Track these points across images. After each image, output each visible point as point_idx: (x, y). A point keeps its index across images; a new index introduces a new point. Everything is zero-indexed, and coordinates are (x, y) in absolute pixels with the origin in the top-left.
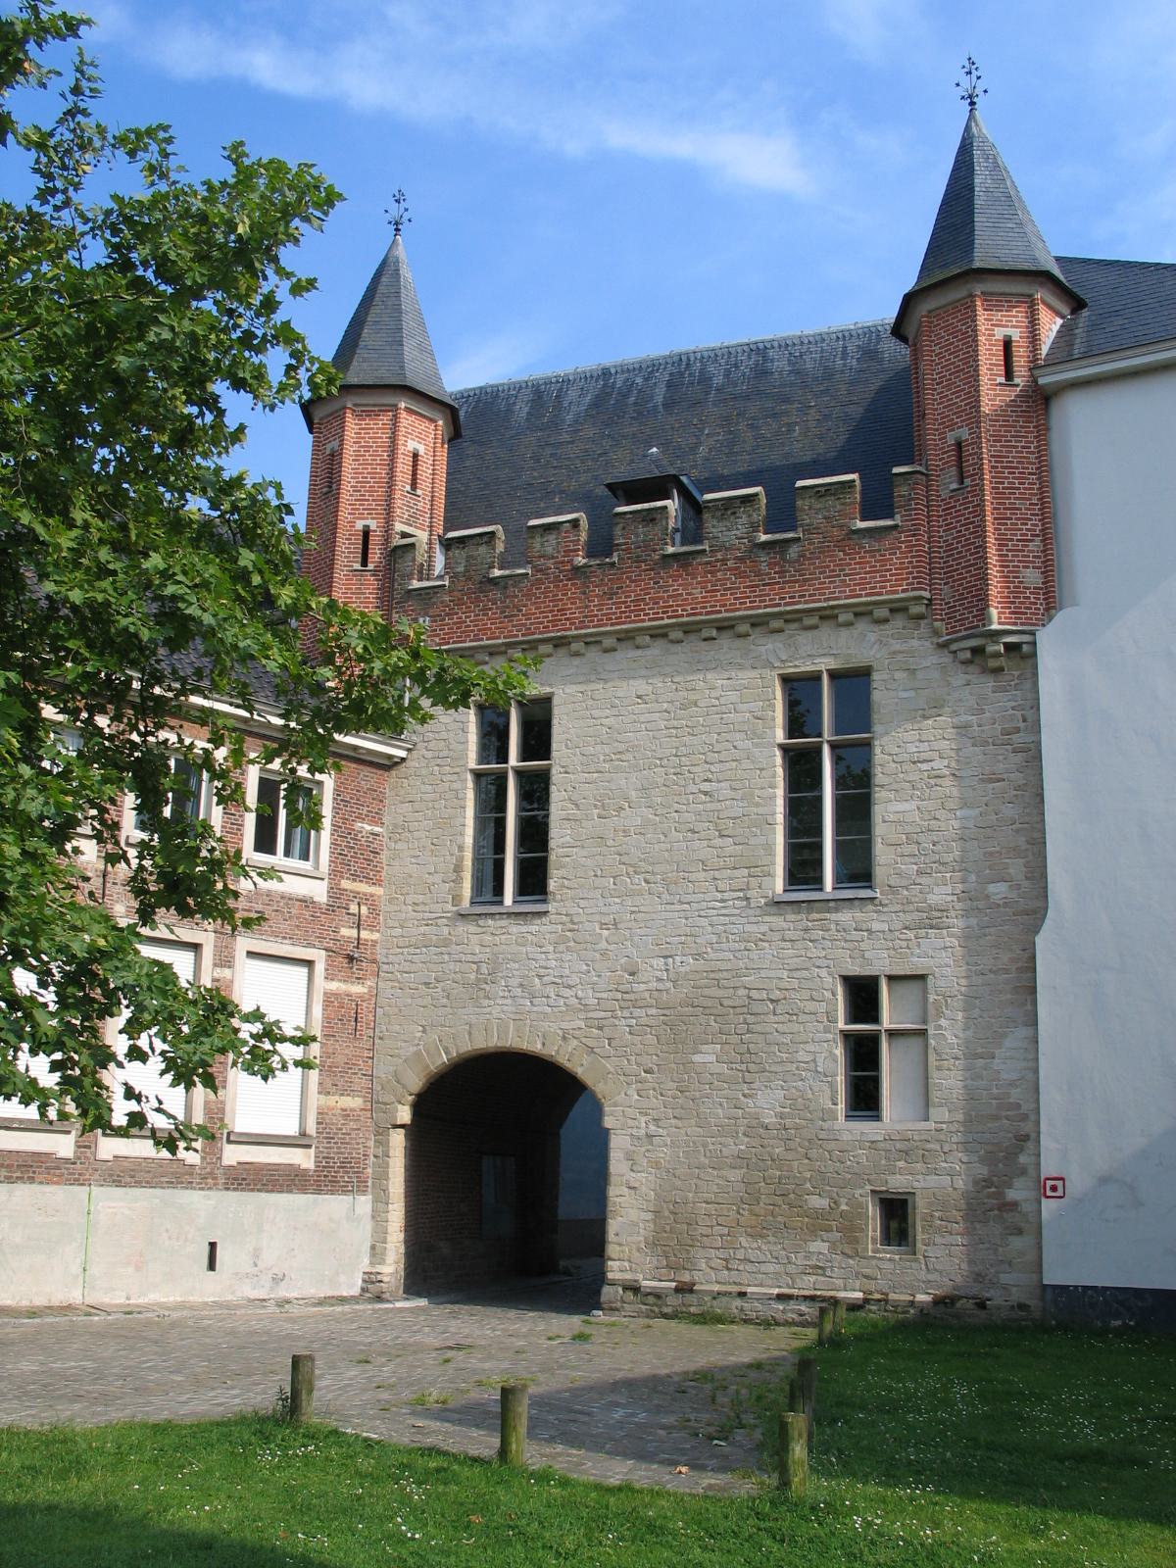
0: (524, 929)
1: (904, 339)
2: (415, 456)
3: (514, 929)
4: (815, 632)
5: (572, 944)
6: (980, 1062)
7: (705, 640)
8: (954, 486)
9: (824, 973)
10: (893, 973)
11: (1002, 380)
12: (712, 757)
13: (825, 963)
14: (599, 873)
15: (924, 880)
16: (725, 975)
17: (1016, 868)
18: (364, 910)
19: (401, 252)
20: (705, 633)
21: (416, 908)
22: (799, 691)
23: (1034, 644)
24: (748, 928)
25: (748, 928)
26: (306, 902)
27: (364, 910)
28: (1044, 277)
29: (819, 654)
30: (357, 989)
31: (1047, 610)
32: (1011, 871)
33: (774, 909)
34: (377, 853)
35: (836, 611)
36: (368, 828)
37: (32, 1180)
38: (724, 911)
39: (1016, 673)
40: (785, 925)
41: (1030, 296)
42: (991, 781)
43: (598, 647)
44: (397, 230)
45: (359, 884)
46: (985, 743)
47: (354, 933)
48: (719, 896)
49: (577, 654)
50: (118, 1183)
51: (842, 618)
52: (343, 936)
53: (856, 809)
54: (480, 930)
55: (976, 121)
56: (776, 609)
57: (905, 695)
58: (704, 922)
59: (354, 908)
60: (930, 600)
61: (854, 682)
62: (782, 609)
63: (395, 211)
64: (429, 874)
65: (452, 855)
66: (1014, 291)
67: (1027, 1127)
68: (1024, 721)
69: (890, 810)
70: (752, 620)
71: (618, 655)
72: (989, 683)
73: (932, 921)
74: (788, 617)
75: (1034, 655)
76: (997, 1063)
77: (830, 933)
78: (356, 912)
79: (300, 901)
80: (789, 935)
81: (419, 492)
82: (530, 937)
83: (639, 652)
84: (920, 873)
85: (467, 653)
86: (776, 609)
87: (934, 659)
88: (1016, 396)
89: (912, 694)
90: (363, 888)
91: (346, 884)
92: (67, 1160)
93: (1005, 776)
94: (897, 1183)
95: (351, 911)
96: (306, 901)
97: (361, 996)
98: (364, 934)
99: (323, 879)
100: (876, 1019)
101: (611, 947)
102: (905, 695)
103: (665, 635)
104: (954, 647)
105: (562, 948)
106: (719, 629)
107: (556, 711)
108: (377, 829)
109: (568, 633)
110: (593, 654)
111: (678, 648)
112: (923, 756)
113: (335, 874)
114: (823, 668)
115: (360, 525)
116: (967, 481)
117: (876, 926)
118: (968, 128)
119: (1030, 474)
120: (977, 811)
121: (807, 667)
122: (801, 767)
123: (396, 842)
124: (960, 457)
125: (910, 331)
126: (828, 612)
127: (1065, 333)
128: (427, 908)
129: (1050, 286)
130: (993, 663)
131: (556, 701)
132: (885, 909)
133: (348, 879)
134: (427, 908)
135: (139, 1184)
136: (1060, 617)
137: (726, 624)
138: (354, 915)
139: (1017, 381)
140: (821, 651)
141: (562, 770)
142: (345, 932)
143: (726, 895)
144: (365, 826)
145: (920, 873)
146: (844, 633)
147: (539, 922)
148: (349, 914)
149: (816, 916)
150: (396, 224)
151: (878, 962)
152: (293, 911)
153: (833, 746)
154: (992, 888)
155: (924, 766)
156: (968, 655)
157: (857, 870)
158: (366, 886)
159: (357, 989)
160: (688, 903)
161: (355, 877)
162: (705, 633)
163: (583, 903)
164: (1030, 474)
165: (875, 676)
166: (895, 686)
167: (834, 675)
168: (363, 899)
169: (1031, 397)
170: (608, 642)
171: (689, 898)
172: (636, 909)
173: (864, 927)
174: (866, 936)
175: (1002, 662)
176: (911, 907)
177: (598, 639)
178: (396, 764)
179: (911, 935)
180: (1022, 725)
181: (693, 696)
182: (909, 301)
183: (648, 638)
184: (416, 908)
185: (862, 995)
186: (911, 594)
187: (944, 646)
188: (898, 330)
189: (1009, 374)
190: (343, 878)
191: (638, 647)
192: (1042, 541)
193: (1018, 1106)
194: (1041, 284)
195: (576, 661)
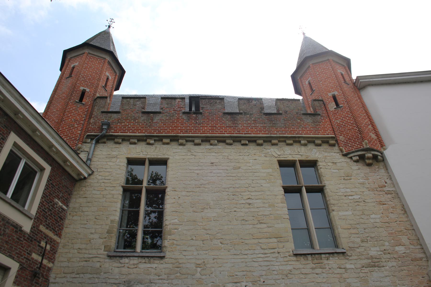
0: (149, 265)
2: (108, 79)
3: (142, 266)
4: (291, 147)
5: (178, 274)
12: (250, 189)
14: (194, 238)
18: (48, 247)
20: (243, 142)
21: (80, 251)
24: (281, 267)
25: (281, 267)
26: (17, 228)
27: (48, 247)
33: (294, 258)
34: (62, 219)
35: (300, 139)
36: (60, 204)
38: (266, 259)
40: (301, 266)
45: (49, 231)
46: (373, 190)
47: (39, 259)
48: (263, 251)
49: (181, 144)
52: (33, 259)
54: (120, 265)
58: (256, 264)
59: (43, 244)
64: (92, 233)
65: (107, 225)
71: (201, 147)
72: (367, 170)
77: (326, 269)
78: (44, 246)
79: (14, 226)
80: (304, 271)
82: (153, 270)
83: (212, 147)
85: (126, 138)
90: (51, 234)
91: (42, 228)
93: (386, 203)
95: (41, 245)
96: (17, 228)
98: (45, 262)
99: (31, 219)
101: (203, 277)
105: (172, 277)
106: (249, 141)
108: (64, 207)
109: (179, 135)
110: (190, 146)
112: (349, 194)
113: (38, 220)
114: (297, 159)
115: (82, 88)
117: (348, 266)
123: (73, 216)
126: (297, 139)
128: (87, 252)
130: (367, 161)
132: (350, 258)
133: (44, 225)
134: (87, 252)
138: (42, 247)
140: (295, 153)
141: (173, 190)
142: (34, 256)
143: (266, 251)
144: (59, 202)
145: (362, 241)
146: (303, 148)
147: (158, 262)
148: (39, 246)
149: (316, 261)
152: (7, 231)
154: (397, 248)
155: (350, 197)
156: (358, 158)
158: (53, 234)
160: (246, 255)
161: (48, 227)
163: (185, 253)
168: (50, 241)
170: (197, 141)
171: (246, 252)
172: (217, 257)
173: (342, 267)
175: (370, 161)
176: (363, 257)
177: (193, 139)
178: (81, 179)
179: (366, 270)
181: (238, 165)
183: (216, 141)
184: (80, 251)
190: (42, 224)
191: (211, 145)
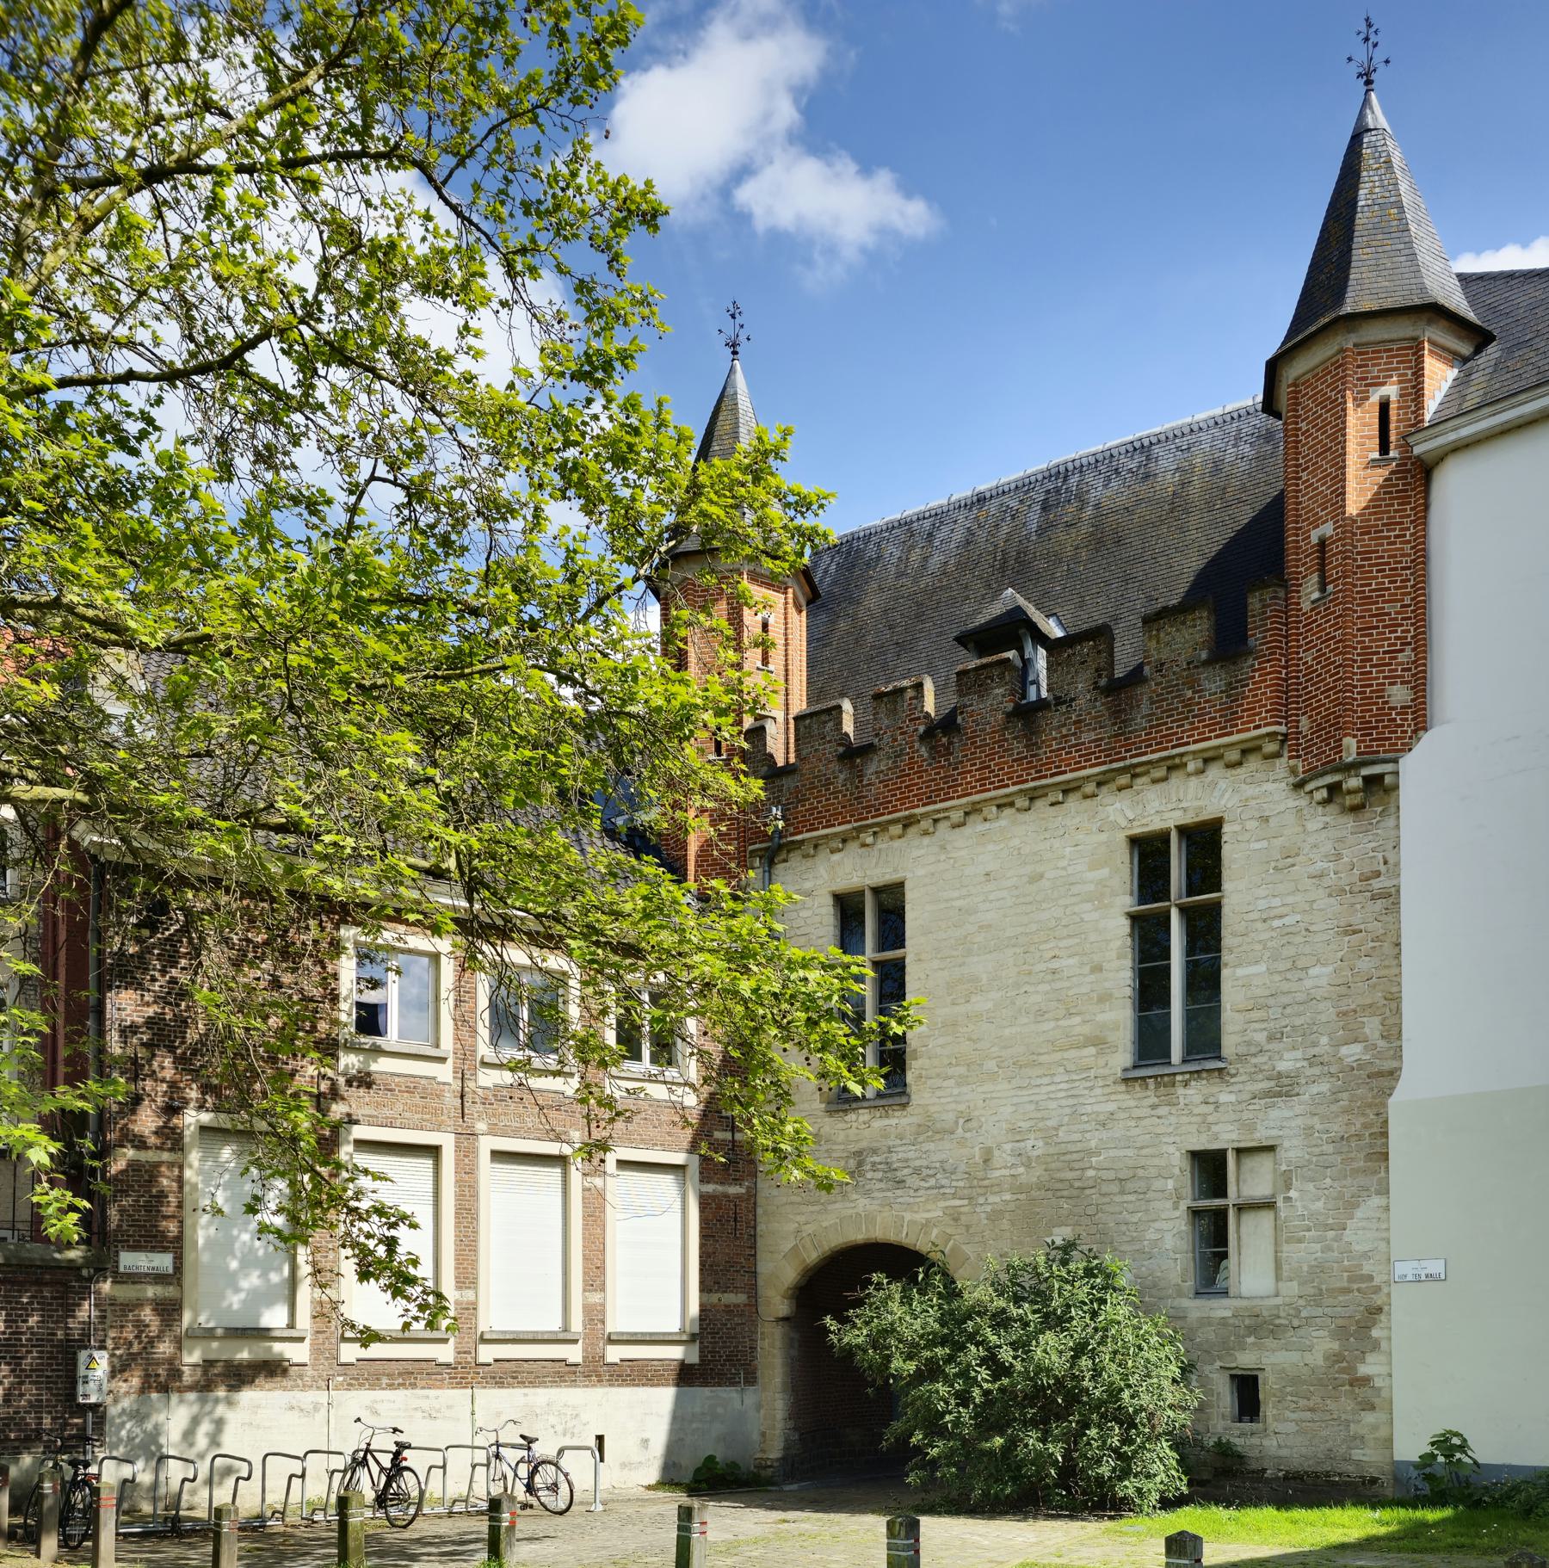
0: (886, 1122)
1: (1278, 416)
6: (1331, 1234)
7: (1052, 805)
8: (1316, 595)
9: (1172, 1149)
10: (1242, 1145)
11: (1376, 455)
13: (1172, 1139)
15: (1275, 1046)
16: (1075, 1156)
17: (1372, 1027)
19: (1377, 117)
22: (1149, 853)
23: (1397, 773)
28: (1435, 311)
29: (1164, 806)
30: (734, 1190)
31: (1415, 731)
32: (1367, 1030)
37: (414, 1386)
39: (1379, 809)
41: (1414, 339)
42: (1346, 933)
43: (1220, 764)
44: (735, 353)
49: (926, 833)
50: (500, 1384)
51: (1191, 767)
53: (1205, 982)
55: (1371, 108)
56: (1121, 764)
57: (1257, 846)
60: (1285, 735)
61: (1204, 841)
62: (1128, 762)
63: (730, 329)
66: (1394, 336)
67: (1379, 1300)
68: (1385, 863)
69: (1240, 980)
70: (1064, 787)
71: (967, 830)
73: (1283, 1088)
74: (1206, 755)
75: (1396, 787)
76: (1348, 1235)
80: (1137, 1113)
81: (771, 667)
83: (987, 825)
84: (1270, 1038)
86: (1121, 764)
87: (1291, 803)
88: (1392, 473)
89: (1264, 844)
92: (448, 1365)
94: (1246, 1360)
97: (739, 1197)
100: (1224, 1195)
102: (1257, 846)
103: (1012, 804)
104: (1309, 787)
107: (910, 896)
111: (1026, 816)
116: (1330, 588)
118: (1361, 116)
119: (1403, 569)
120: (1331, 968)
121: (1156, 825)
122: (1148, 936)
124: (1323, 559)
125: (1283, 402)
127: (1460, 384)
129: (1443, 323)
131: (908, 886)
135: (522, 1384)
136: (1426, 738)
137: (1072, 785)
139: (1392, 454)
150: (734, 345)
151: (1225, 1136)
153: (1183, 910)
154: (1344, 1050)
155: (1276, 923)
157: (1205, 1040)
159: (734, 1190)
162: (1051, 798)
164: (1403, 569)
165: (1226, 828)
166: (1247, 836)
167: (1183, 830)
169: (1409, 471)
173: (1211, 1100)
174: (1203, 1113)
180: (1382, 868)
182: (1273, 368)
185: (1210, 1168)
186: (1264, 730)
187: (1298, 786)
188: (1269, 405)
189: (1384, 447)
192: (1414, 650)
193: (1371, 1278)
194: (1430, 322)
195: (926, 840)
